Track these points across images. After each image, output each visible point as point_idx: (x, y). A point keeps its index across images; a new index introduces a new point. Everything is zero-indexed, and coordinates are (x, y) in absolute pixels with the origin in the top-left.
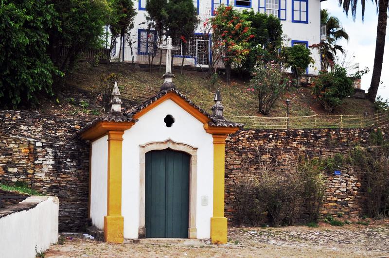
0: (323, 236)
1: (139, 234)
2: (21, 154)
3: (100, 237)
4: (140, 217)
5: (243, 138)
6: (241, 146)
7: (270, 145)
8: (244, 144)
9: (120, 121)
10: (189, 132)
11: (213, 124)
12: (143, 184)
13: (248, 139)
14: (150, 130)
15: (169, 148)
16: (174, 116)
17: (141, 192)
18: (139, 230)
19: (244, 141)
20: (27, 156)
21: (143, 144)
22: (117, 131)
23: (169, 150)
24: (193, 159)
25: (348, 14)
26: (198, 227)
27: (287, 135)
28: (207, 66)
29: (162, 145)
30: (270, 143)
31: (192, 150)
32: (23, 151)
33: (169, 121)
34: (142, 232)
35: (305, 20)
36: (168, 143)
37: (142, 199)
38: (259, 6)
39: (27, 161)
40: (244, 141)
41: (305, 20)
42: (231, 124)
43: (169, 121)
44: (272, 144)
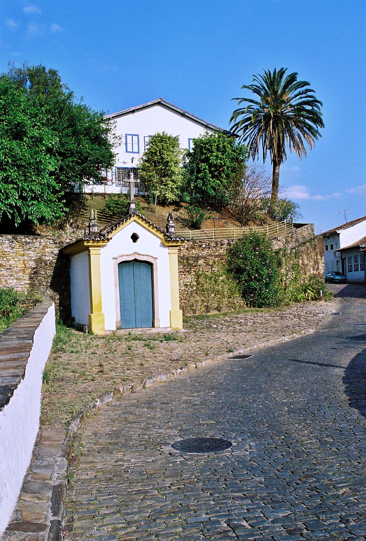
1: (116, 326)
3: (80, 328)
7: (203, 252)
10: (150, 245)
13: (187, 249)
14: (120, 244)
16: (138, 234)
18: (116, 323)
21: (115, 256)
23: (136, 260)
24: (154, 266)
25: (321, 133)
29: (130, 257)
32: (19, 266)
33: (135, 238)
34: (118, 325)
35: (137, 151)
38: (138, 138)
41: (137, 151)
43: (135, 238)
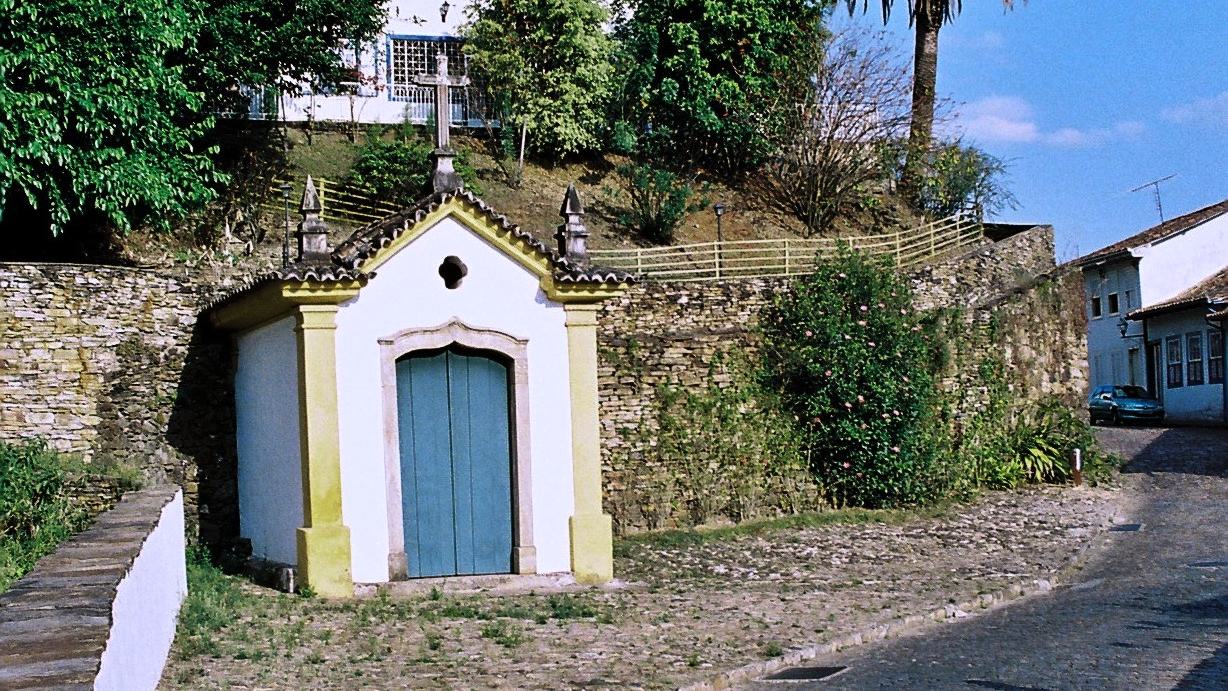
0: (834, 548)
2: (62, 377)
4: (529, 495)
5: (615, 308)
6: (611, 327)
8: (617, 323)
9: (328, 279)
10: (504, 298)
11: (566, 277)
12: (393, 441)
13: (628, 310)
15: (455, 342)
16: (464, 260)
17: (391, 460)
18: (390, 558)
19: (617, 316)
20: (75, 381)
21: (386, 335)
22: (318, 304)
23: (455, 348)
24: (517, 367)
26: (538, 541)
27: (724, 294)
28: (342, 83)
29: (437, 336)
30: (682, 316)
31: (514, 346)
32: (64, 368)
33: (452, 272)
34: (397, 565)
36: (452, 329)
37: (393, 478)
39: (78, 393)
40: (617, 316)
42: (613, 275)
43: (452, 272)
44: (689, 320)
